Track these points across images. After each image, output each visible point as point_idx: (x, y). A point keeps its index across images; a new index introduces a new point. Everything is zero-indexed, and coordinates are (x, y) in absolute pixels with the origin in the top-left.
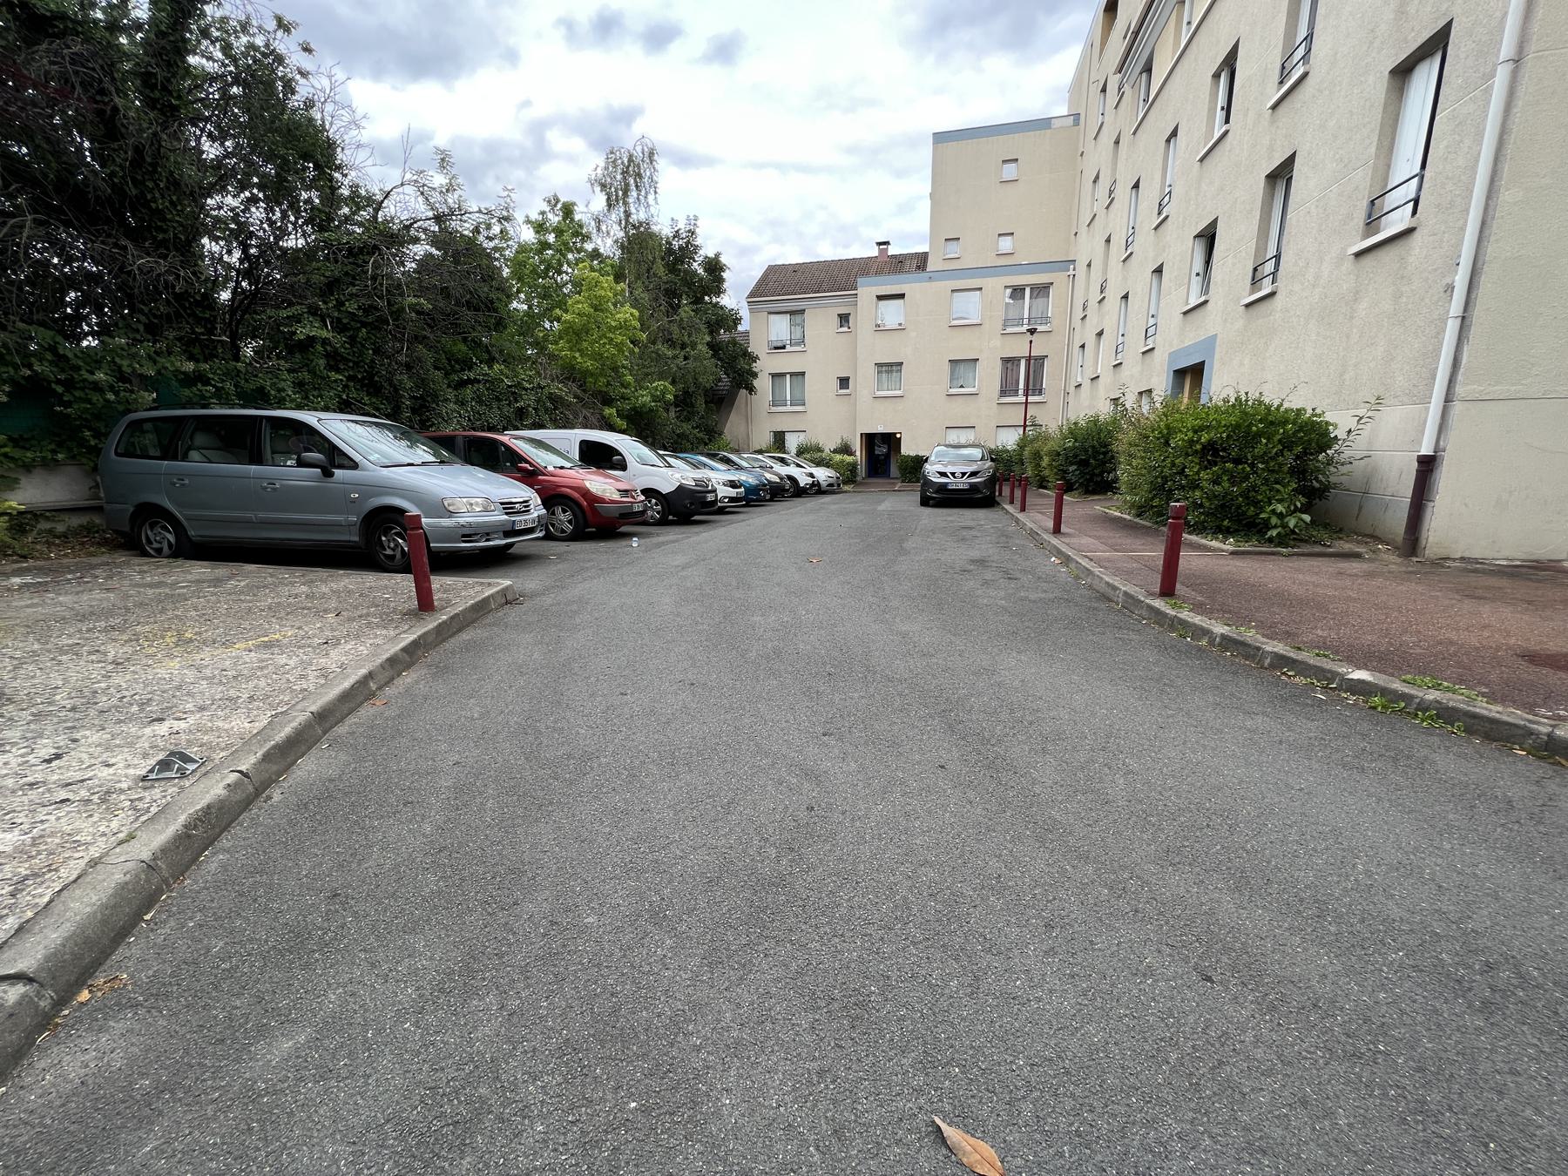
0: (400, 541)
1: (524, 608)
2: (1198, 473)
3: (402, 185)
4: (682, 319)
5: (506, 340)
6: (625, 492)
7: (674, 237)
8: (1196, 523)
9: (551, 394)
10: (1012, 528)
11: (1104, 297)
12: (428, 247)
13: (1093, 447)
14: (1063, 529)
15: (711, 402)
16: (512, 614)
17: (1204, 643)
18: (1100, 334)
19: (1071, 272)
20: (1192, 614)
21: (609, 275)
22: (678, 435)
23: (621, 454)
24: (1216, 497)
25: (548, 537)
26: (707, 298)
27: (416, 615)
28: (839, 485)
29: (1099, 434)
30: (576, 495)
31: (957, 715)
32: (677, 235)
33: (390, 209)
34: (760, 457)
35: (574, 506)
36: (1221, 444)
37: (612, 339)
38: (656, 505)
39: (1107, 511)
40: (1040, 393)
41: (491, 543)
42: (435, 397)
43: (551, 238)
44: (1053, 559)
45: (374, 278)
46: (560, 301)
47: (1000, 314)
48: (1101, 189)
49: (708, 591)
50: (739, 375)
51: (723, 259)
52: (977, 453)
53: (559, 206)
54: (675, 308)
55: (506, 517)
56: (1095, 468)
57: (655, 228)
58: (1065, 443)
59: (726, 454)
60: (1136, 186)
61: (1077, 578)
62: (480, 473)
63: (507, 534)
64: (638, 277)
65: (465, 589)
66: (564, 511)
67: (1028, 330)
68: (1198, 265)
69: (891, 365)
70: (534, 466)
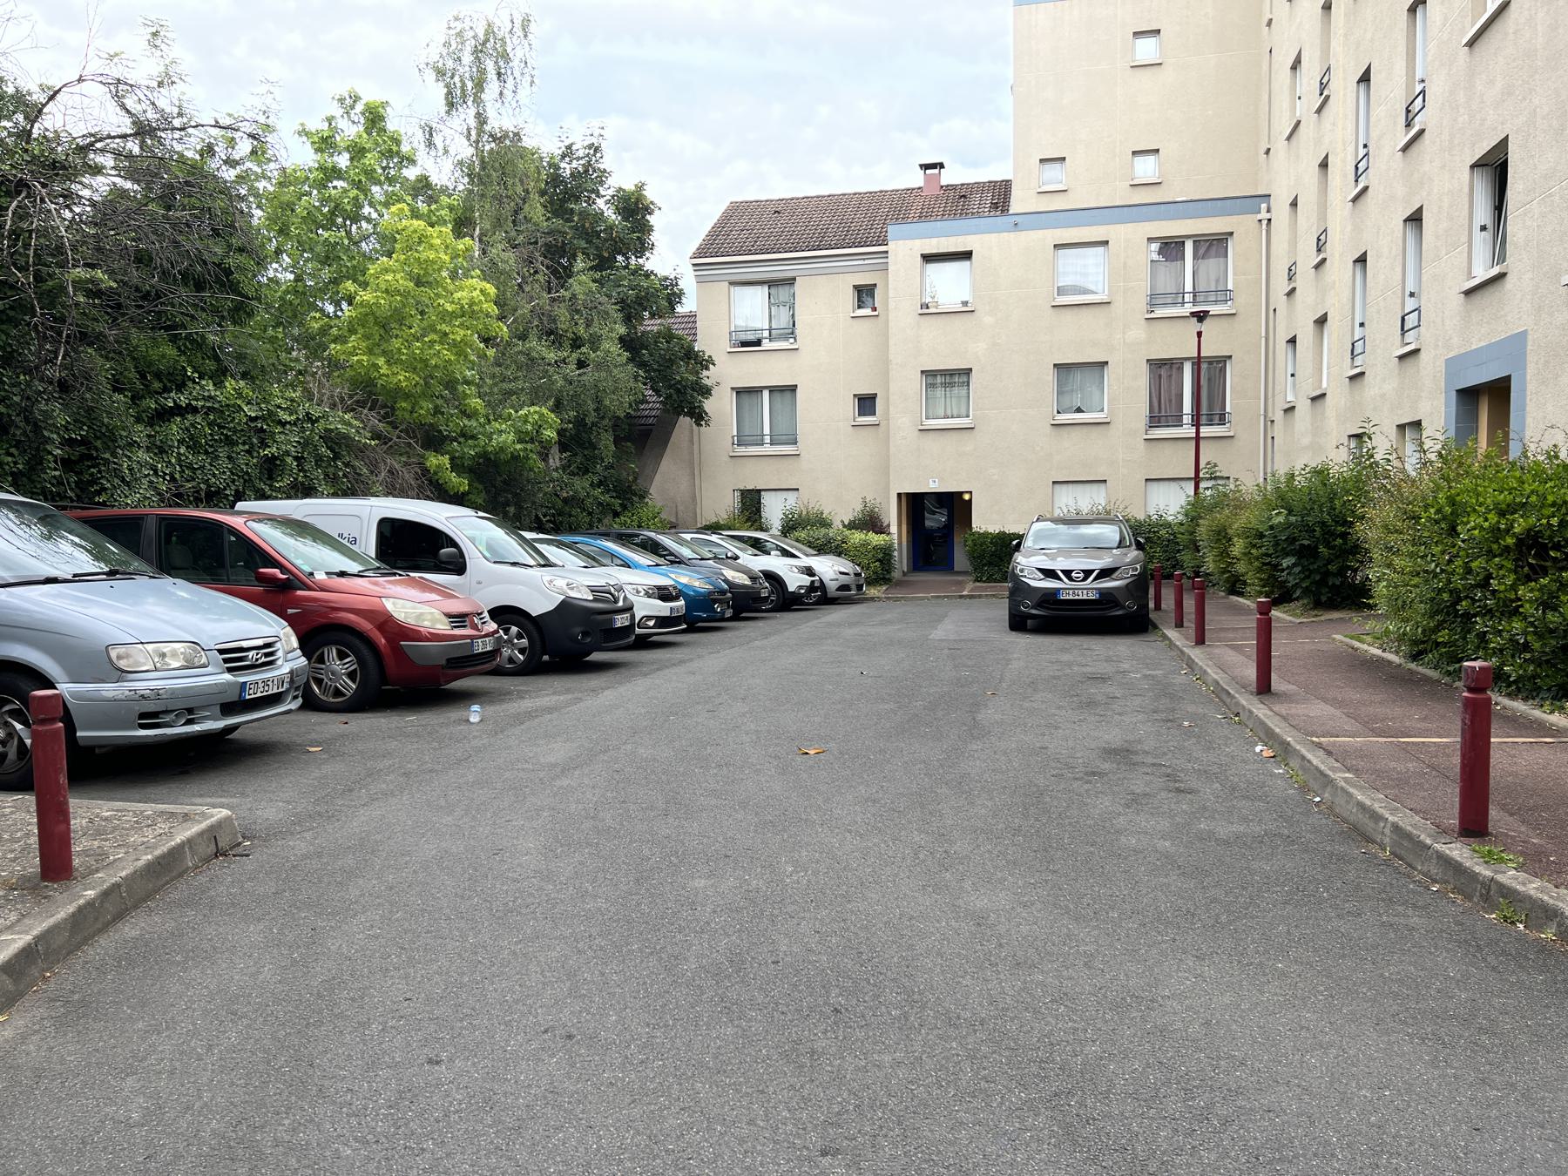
0: (18, 726)
1: (249, 864)
2: (1514, 588)
3: (80, 80)
4: (574, 296)
5: (253, 338)
6: (459, 619)
7: (563, 156)
8: (1520, 678)
9: (331, 431)
10: (1181, 678)
11: (1324, 260)
12: (118, 180)
13: (1323, 524)
14: (1276, 683)
15: (627, 439)
16: (226, 878)
17: (1549, 934)
18: (1321, 321)
19: (1264, 215)
20: (1522, 875)
21: (445, 223)
22: (565, 501)
23: (454, 544)
24: (1551, 631)
25: (311, 704)
26: (620, 258)
27: (34, 889)
28: (860, 587)
29: (1331, 500)
30: (365, 625)
31: (1082, 1104)
32: (568, 153)
33: (51, 121)
34: (714, 538)
35: (357, 642)
36: (1551, 538)
37: (446, 334)
38: (519, 636)
39: (1357, 644)
40: (1222, 420)
41: (197, 728)
42: (110, 438)
43: (343, 161)
44: (1258, 749)
45: (15, 234)
46: (354, 267)
47: (1143, 288)
48: (1305, 80)
49: (609, 822)
50: (678, 391)
51: (650, 194)
52: (1110, 533)
53: (359, 107)
54: (562, 275)
55: (228, 677)
56: (1329, 562)
57: (527, 142)
58: (1270, 519)
59: (652, 535)
60: (1365, 78)
61: (1304, 789)
62: (181, 589)
63: (228, 709)
64: (498, 223)
65: (137, 827)
66: (342, 656)
67: (1193, 314)
68: (1483, 214)
69: (951, 373)
70: (289, 572)
